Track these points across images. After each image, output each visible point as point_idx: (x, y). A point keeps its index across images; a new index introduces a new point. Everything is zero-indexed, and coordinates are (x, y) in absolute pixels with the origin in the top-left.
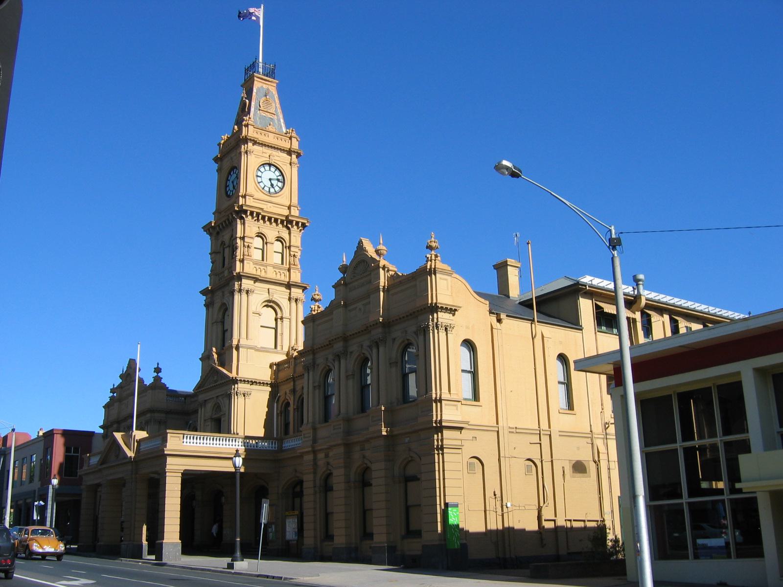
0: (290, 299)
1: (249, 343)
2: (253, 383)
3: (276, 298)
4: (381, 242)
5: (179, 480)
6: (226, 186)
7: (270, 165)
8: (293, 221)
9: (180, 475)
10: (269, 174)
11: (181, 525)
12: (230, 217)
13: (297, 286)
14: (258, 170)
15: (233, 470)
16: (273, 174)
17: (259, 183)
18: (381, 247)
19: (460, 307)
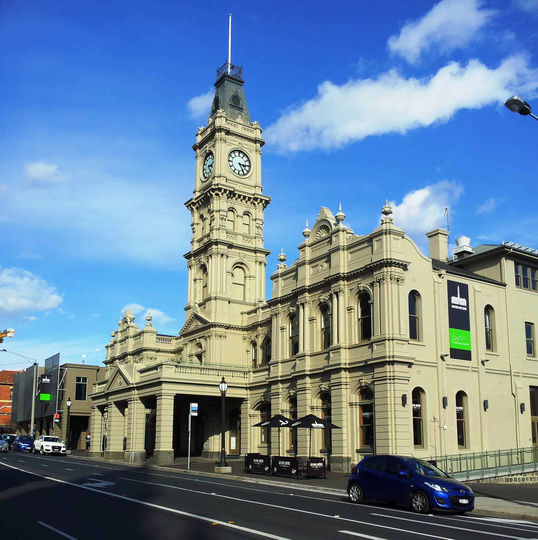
0: (256, 262)
1: (257, 241)
2: (228, 327)
3: (245, 261)
4: (340, 209)
5: (172, 402)
6: (204, 170)
7: (240, 152)
8: (258, 198)
9: (173, 398)
10: (238, 159)
11: (174, 426)
12: (208, 194)
13: (261, 252)
14: (230, 155)
15: (220, 395)
16: (243, 160)
17: (230, 166)
18: (340, 214)
19: (410, 263)
